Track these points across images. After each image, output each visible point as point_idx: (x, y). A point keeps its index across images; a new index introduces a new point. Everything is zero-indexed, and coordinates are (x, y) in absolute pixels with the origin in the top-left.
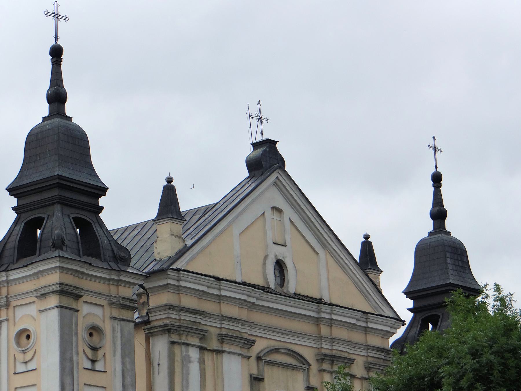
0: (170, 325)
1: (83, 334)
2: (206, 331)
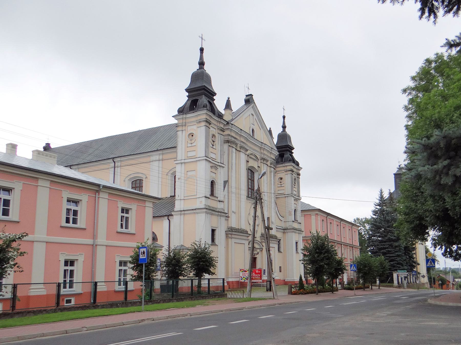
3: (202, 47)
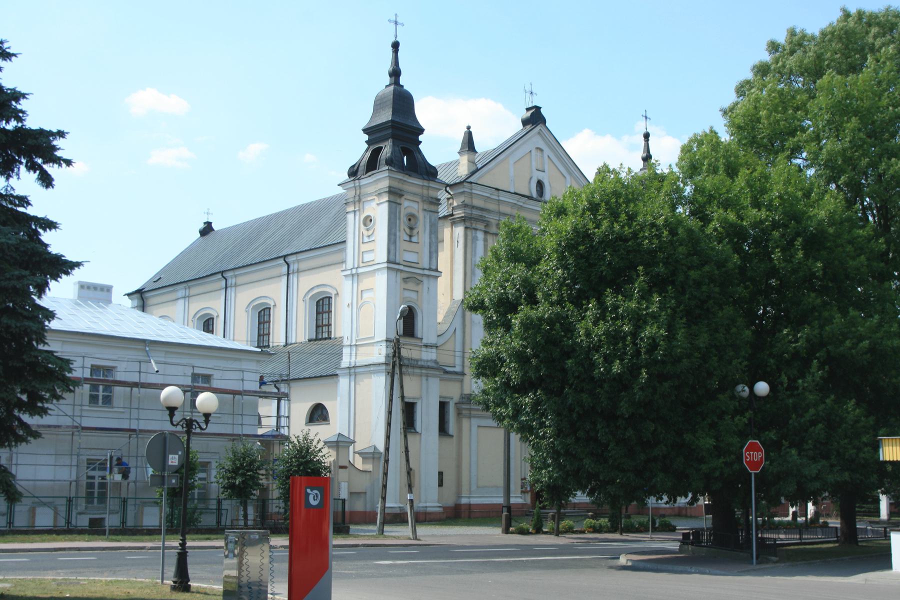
1: (404, 219)
2: (488, 221)
3: (397, 39)
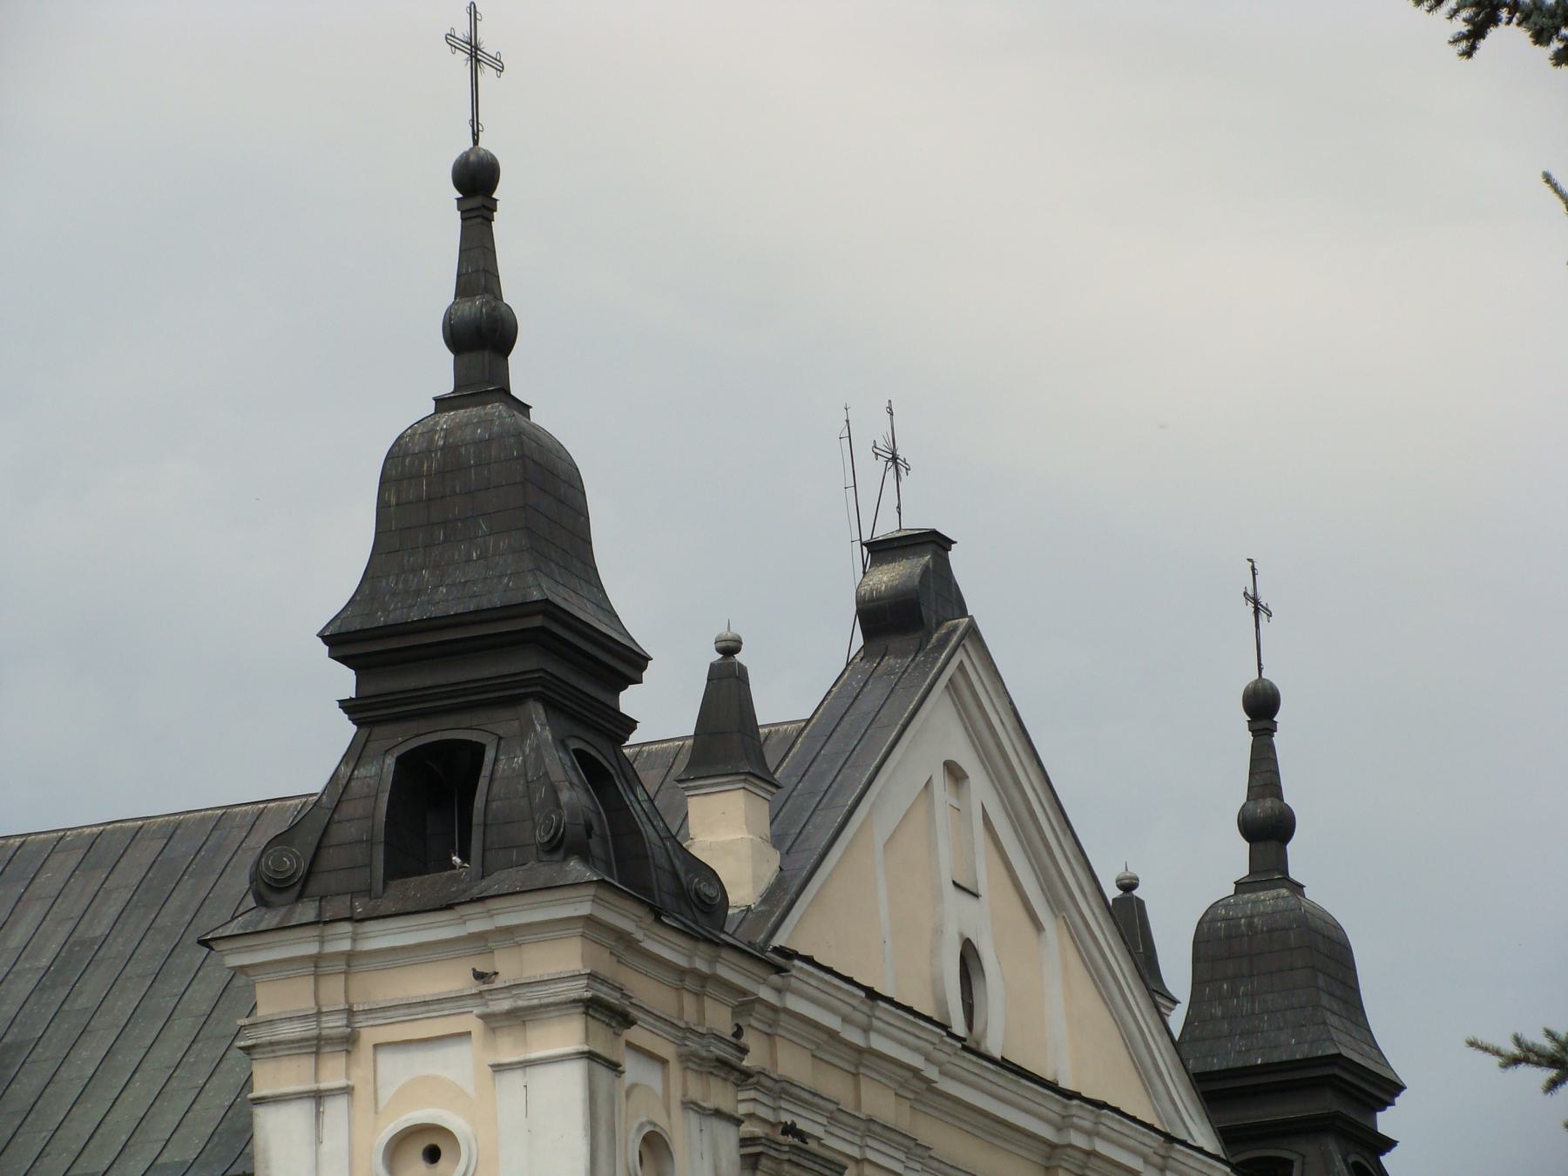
0: (763, 1141)
